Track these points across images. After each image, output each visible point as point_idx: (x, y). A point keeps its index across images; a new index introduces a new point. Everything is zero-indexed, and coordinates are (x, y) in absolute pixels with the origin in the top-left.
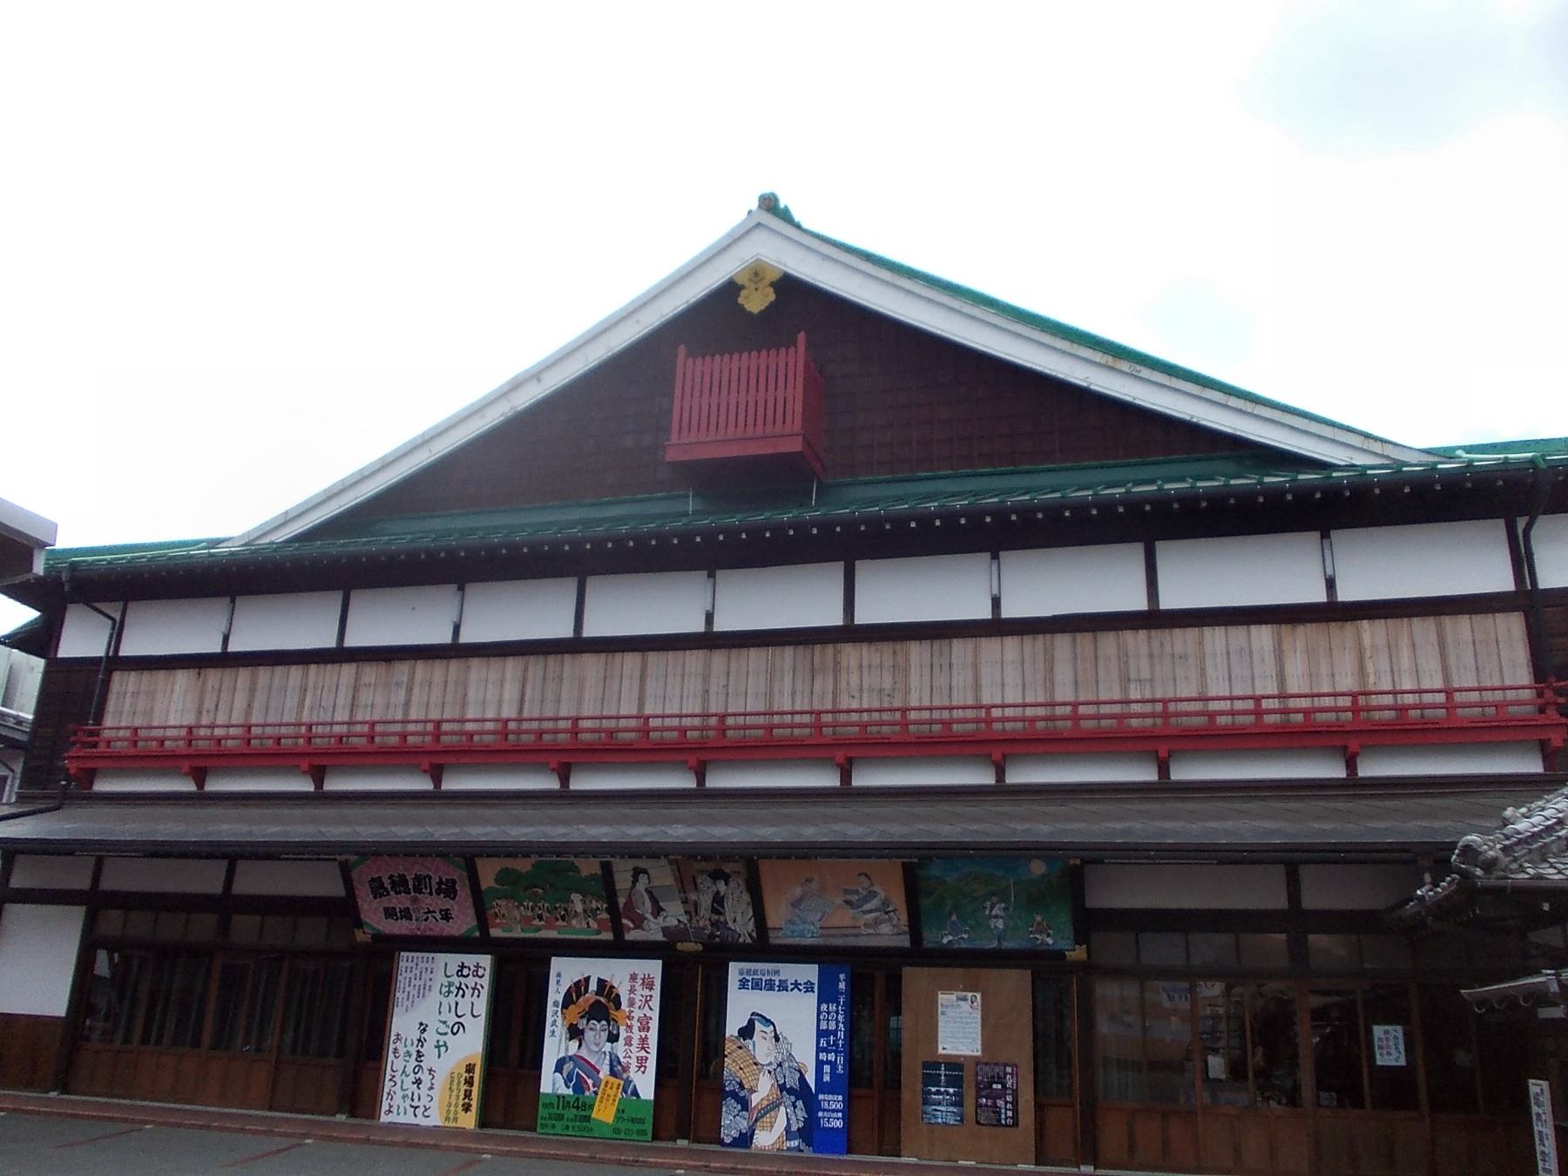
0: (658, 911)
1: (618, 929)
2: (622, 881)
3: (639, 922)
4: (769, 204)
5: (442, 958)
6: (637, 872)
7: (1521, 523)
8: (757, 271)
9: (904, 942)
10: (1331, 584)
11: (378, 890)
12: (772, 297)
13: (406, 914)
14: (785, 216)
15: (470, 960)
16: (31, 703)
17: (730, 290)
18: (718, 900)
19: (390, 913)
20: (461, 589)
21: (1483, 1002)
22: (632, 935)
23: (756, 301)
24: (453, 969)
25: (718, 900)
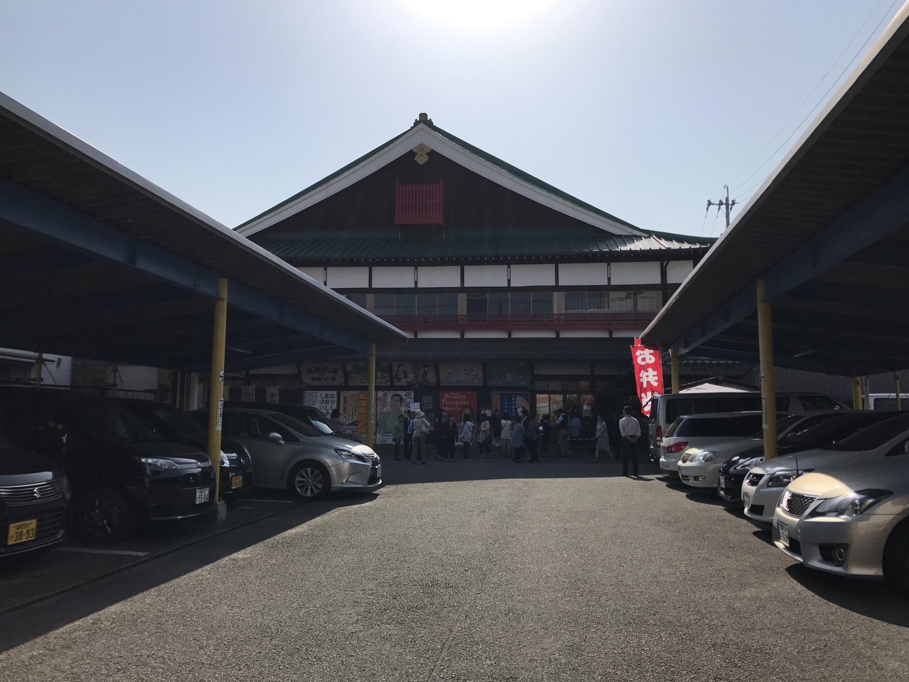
0: (406, 376)
1: (392, 382)
2: (395, 368)
3: (399, 380)
4: (423, 116)
5: (319, 392)
6: (400, 366)
7: (665, 262)
8: (422, 147)
9: (481, 384)
10: (609, 279)
11: (310, 371)
12: (427, 159)
13: (319, 379)
14: (429, 124)
15: (330, 393)
16: (465, 308)
17: (411, 154)
18: (425, 373)
19: (313, 379)
20: (325, 269)
21: (156, 471)
22: (397, 384)
23: (422, 160)
24: (324, 396)
25: (425, 373)
